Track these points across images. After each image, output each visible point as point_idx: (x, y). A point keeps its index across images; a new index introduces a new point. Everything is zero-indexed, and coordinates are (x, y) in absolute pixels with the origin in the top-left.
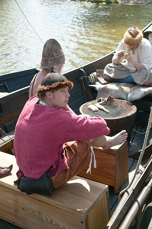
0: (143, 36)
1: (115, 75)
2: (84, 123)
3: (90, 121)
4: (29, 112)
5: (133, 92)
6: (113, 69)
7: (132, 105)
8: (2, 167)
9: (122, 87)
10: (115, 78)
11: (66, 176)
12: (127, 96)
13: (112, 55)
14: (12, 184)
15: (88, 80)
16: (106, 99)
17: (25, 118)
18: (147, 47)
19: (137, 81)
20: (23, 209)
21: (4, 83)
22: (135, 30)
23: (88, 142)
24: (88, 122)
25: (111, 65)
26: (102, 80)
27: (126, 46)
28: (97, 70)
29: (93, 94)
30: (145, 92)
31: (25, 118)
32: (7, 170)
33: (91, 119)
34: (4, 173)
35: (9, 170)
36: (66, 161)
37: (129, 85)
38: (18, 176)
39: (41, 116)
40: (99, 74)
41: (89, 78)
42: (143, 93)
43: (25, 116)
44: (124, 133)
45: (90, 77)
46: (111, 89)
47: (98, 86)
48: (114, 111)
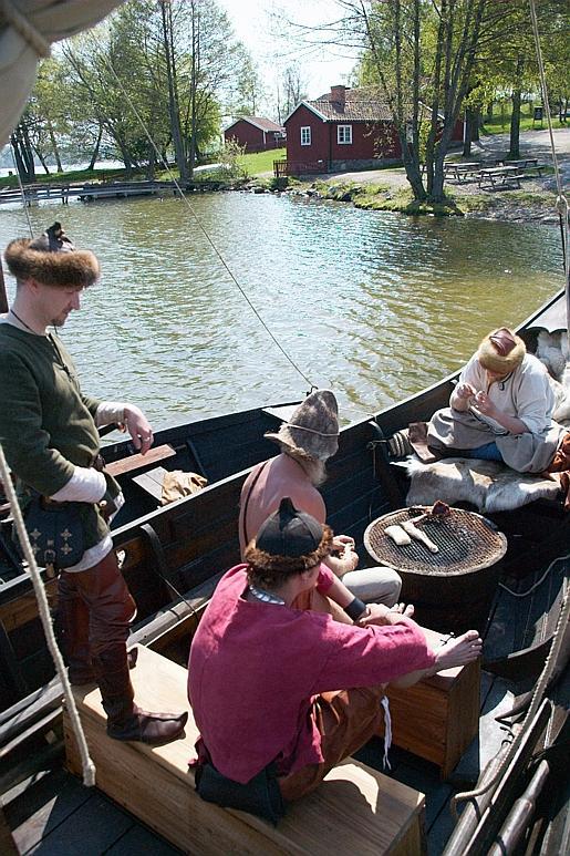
0: (525, 350)
1: (455, 441)
2: (366, 650)
3: (384, 641)
4: (225, 613)
5: (499, 491)
6: (451, 424)
7: (496, 530)
8: (163, 714)
9: (473, 473)
10: (456, 447)
11: (316, 774)
12: (484, 499)
13: (450, 386)
14: (185, 769)
15: (389, 449)
16: (430, 509)
17: (214, 628)
18: (536, 377)
19: (512, 460)
20: (210, 831)
21: (187, 444)
22: (507, 336)
23: (376, 693)
24: (376, 645)
25: (447, 412)
26: (423, 451)
27: (483, 373)
28: (411, 425)
29: (394, 491)
30: (529, 495)
31: (214, 628)
32: (173, 725)
33: (386, 635)
34: (166, 733)
35: (178, 724)
36: (316, 742)
37: (489, 468)
38: (198, 751)
39: (253, 632)
40: (417, 433)
41: (392, 444)
42: (525, 495)
43: (214, 623)
44: (475, 638)
45: (395, 442)
46: (446, 479)
47: (413, 466)
48: (451, 548)
